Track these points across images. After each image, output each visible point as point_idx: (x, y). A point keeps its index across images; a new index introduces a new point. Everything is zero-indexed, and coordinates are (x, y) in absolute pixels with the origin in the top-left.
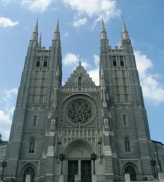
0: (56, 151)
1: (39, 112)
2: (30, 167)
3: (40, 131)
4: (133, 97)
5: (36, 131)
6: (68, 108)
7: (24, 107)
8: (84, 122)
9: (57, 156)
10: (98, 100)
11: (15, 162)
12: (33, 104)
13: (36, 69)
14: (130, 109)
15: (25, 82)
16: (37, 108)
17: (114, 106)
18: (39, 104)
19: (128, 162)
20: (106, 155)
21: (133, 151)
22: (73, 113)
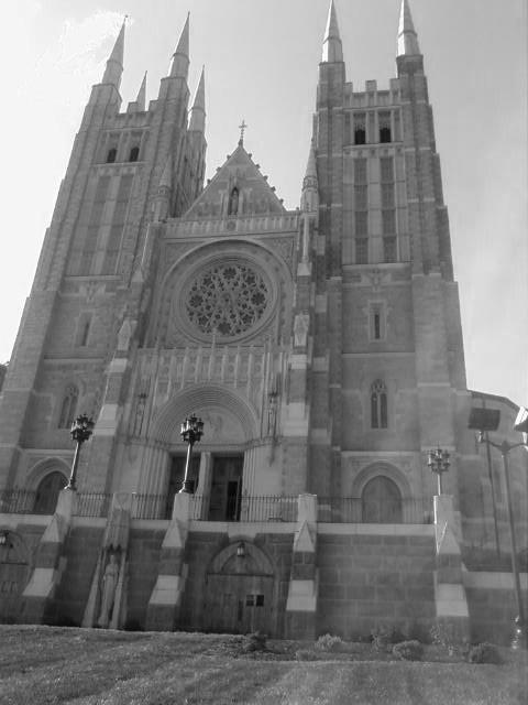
0: (126, 419)
2: (57, 472)
3: (94, 361)
4: (411, 243)
8: (239, 331)
12: (84, 278)
14: (399, 283)
16: (379, 279)
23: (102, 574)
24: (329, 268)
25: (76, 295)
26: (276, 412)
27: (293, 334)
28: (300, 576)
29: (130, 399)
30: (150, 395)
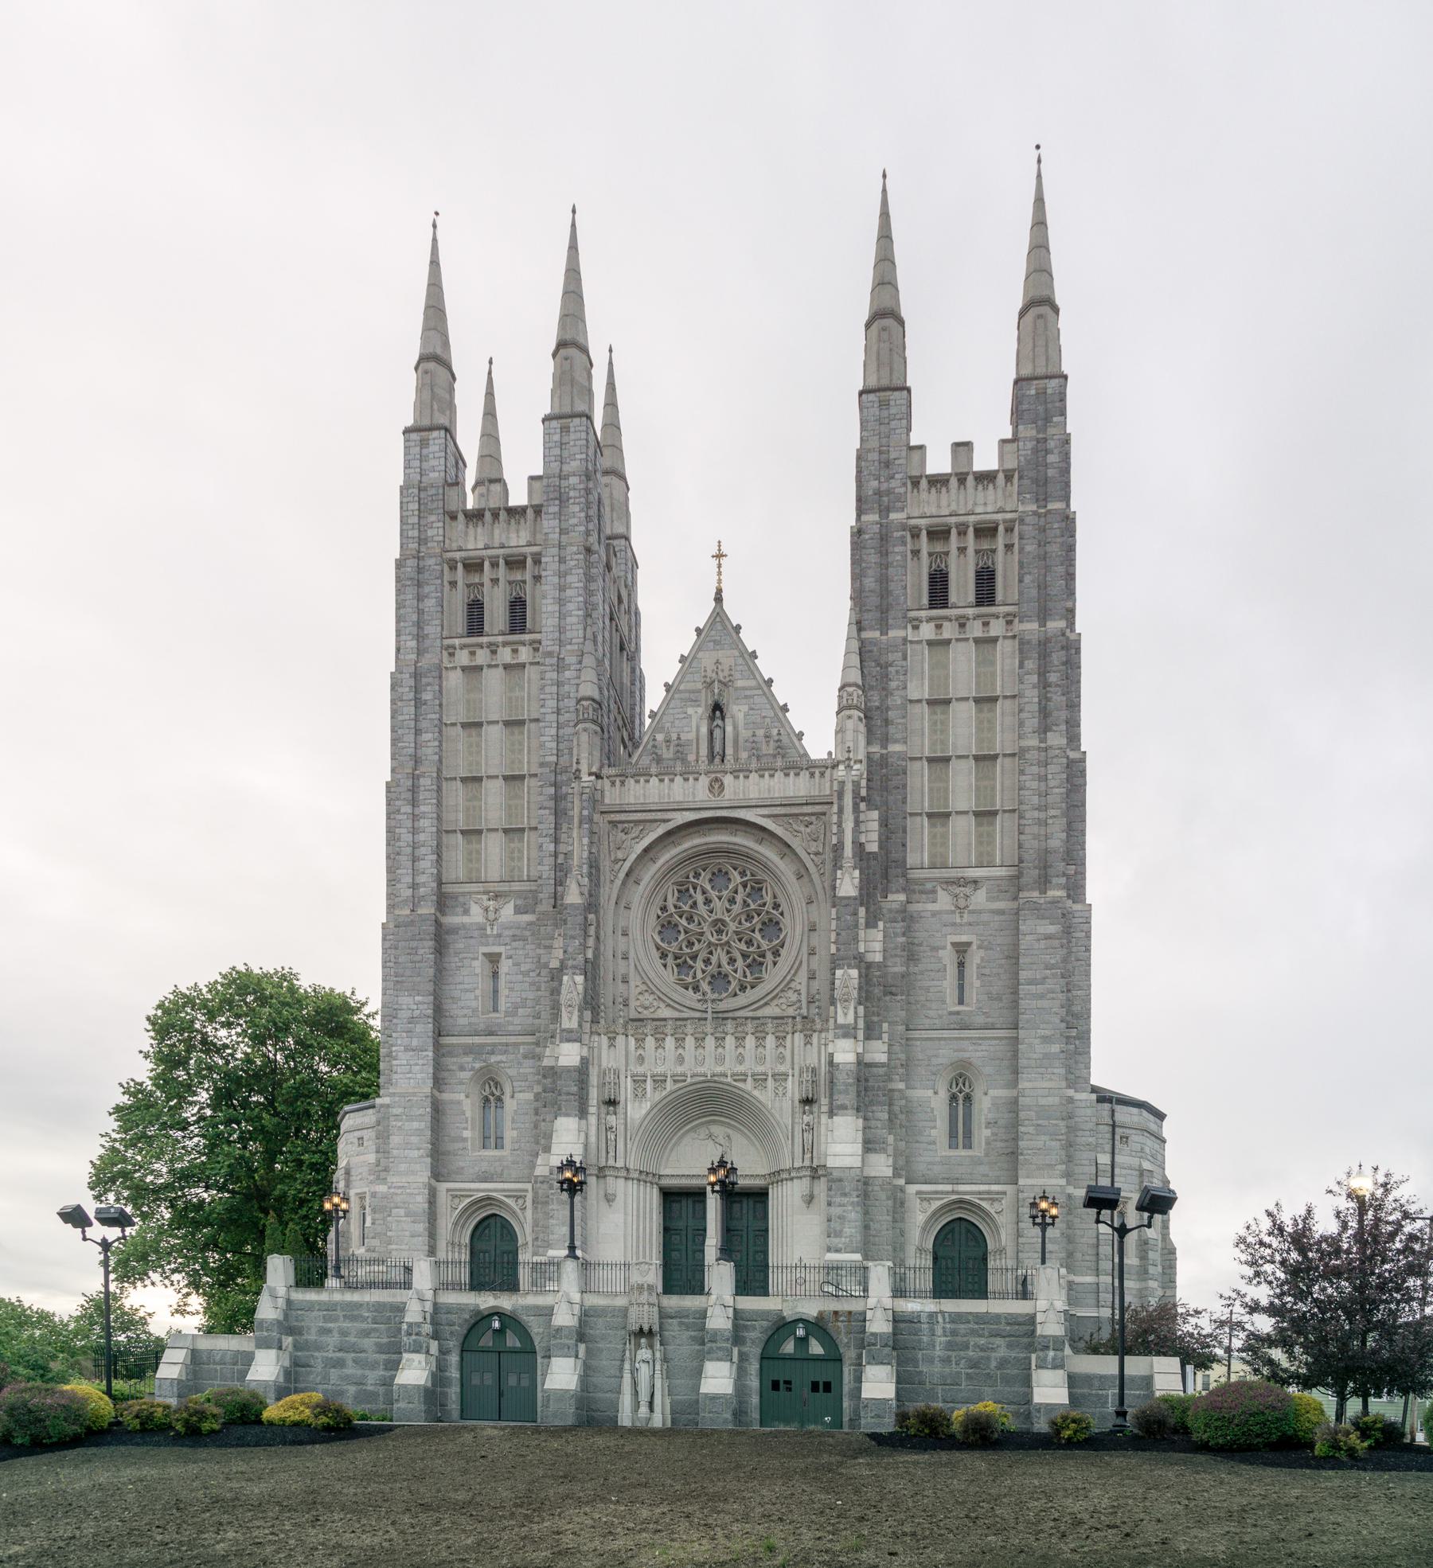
0: (593, 1139)
1: (507, 933)
3: (521, 1039)
5: (504, 1039)
6: (659, 902)
7: (427, 909)
8: (743, 988)
9: (603, 1164)
10: (817, 854)
11: (416, 1191)
13: (465, 652)
15: (411, 751)
17: (904, 890)
18: (504, 887)
19: (955, 1202)
20: (831, 1163)
21: (988, 1143)
22: (682, 937)
23: (633, 1361)
24: (886, 875)
25: (466, 919)
26: (810, 1128)
27: (833, 1002)
28: (875, 1360)
29: (592, 1110)
30: (622, 1099)
